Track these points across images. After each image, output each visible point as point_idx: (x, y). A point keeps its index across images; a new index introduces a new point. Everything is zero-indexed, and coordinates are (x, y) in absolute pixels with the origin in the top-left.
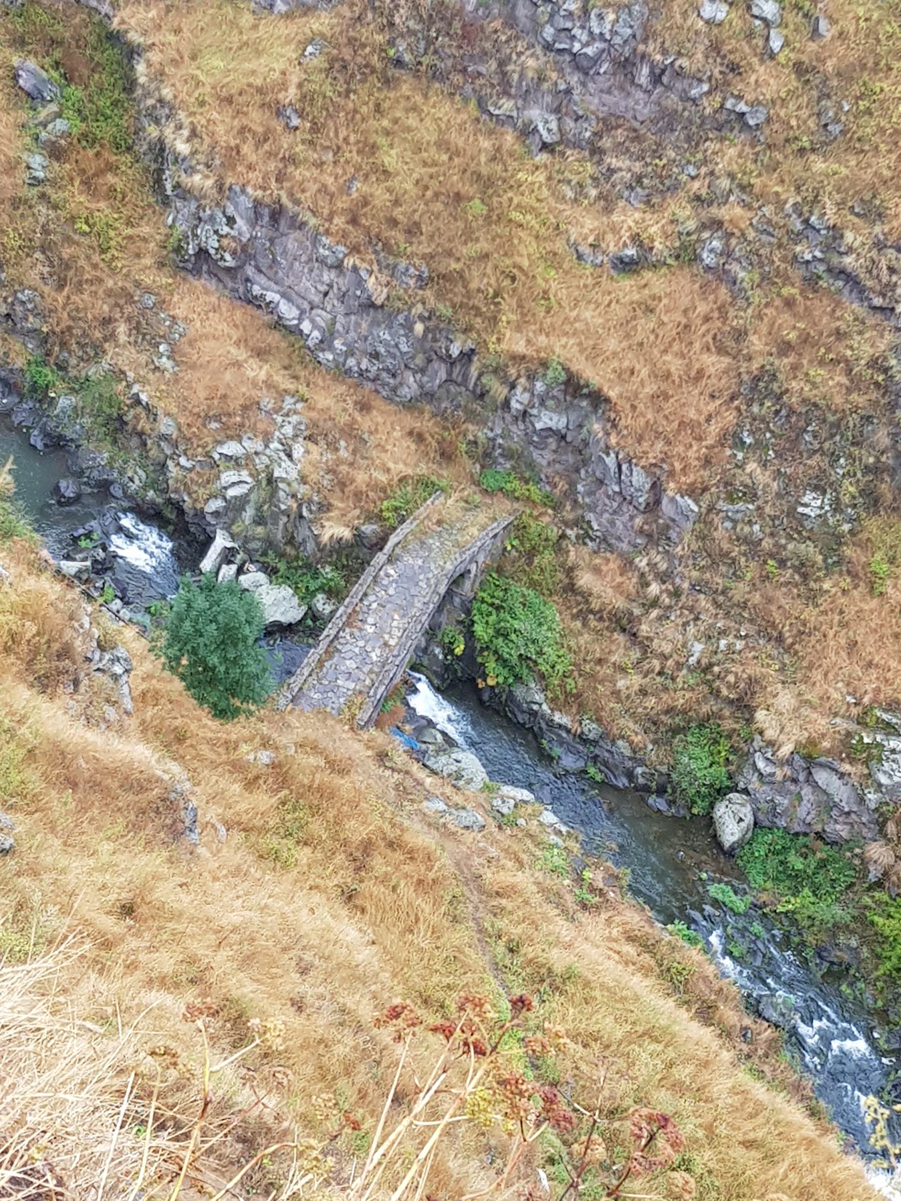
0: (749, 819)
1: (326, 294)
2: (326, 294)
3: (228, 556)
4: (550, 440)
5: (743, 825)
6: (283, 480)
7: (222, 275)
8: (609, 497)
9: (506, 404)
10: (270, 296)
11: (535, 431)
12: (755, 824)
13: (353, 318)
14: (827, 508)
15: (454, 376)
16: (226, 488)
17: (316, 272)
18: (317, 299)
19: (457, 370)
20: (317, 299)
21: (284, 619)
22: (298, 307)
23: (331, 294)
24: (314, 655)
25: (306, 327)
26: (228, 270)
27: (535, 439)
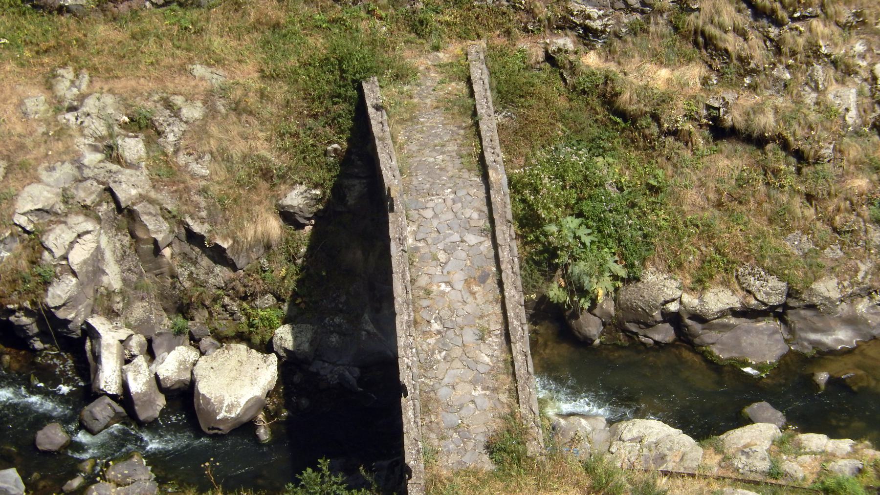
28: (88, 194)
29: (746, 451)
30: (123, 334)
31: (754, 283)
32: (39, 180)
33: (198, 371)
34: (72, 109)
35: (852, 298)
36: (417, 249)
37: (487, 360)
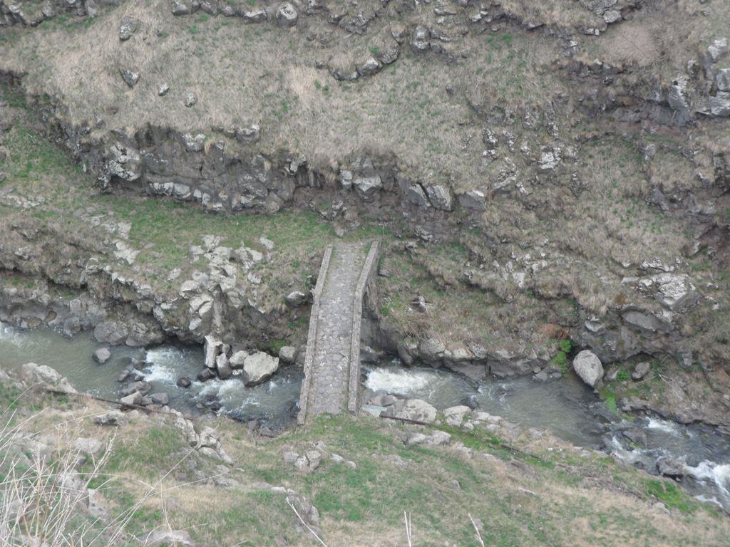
0: (598, 363)
1: (201, 169)
2: (201, 169)
3: (219, 351)
4: (375, 194)
5: (596, 367)
6: (228, 290)
7: (132, 186)
8: (426, 212)
9: (339, 184)
10: (167, 186)
11: (363, 193)
12: (603, 364)
13: (224, 176)
14: (559, 159)
15: (300, 183)
16: (198, 311)
17: (189, 158)
18: (197, 175)
19: (300, 179)
20: (197, 175)
21: (268, 372)
22: (187, 184)
23: (205, 167)
24: (305, 383)
25: (197, 194)
26: (135, 182)
27: (366, 198)
28: (210, 286)
29: (453, 416)
30: (219, 343)
31: (474, 348)
32: (192, 279)
33: (246, 361)
34: (210, 251)
35: (516, 359)
36: (322, 320)
37: (341, 368)
